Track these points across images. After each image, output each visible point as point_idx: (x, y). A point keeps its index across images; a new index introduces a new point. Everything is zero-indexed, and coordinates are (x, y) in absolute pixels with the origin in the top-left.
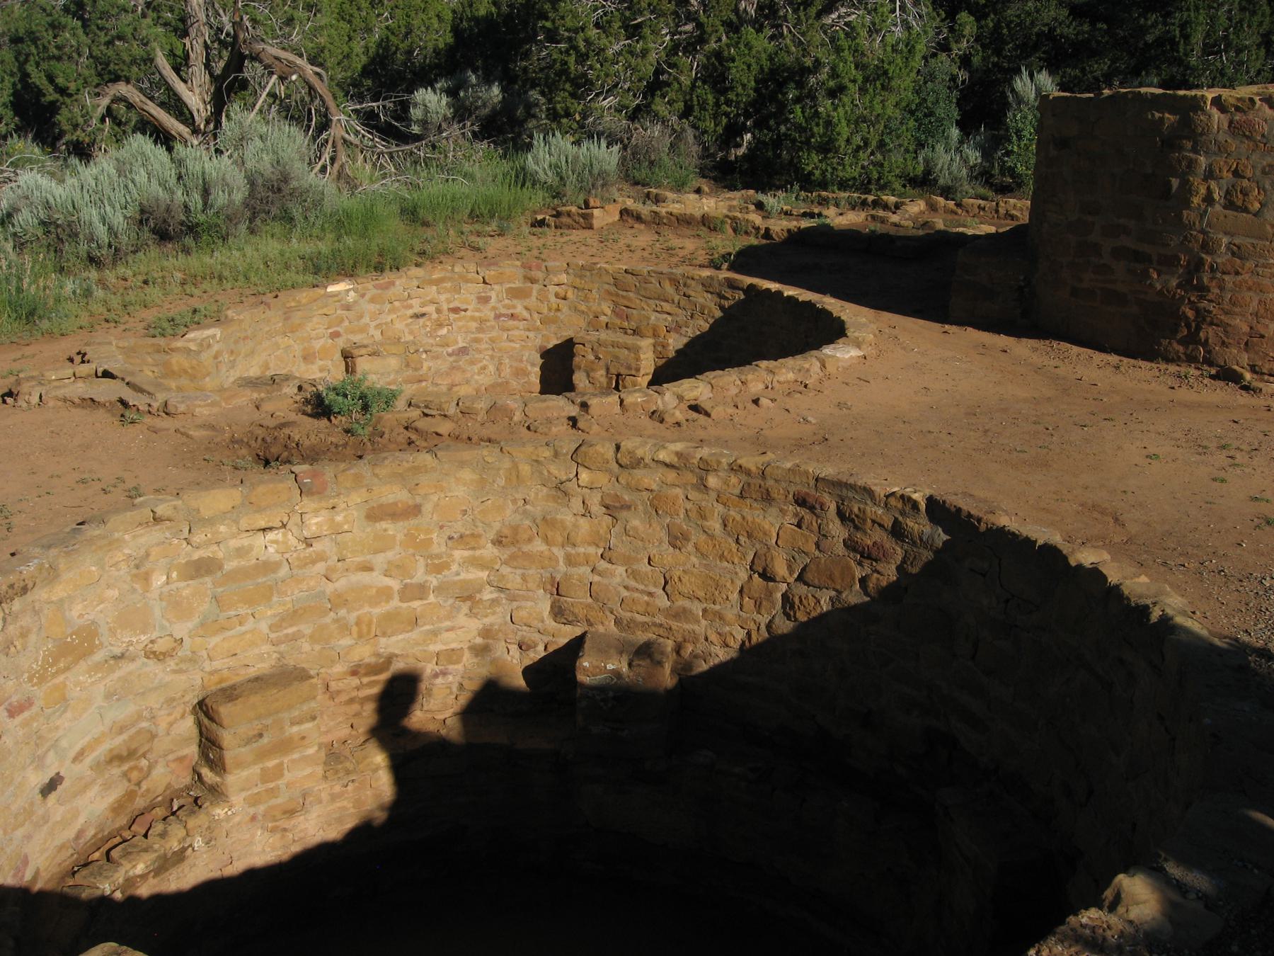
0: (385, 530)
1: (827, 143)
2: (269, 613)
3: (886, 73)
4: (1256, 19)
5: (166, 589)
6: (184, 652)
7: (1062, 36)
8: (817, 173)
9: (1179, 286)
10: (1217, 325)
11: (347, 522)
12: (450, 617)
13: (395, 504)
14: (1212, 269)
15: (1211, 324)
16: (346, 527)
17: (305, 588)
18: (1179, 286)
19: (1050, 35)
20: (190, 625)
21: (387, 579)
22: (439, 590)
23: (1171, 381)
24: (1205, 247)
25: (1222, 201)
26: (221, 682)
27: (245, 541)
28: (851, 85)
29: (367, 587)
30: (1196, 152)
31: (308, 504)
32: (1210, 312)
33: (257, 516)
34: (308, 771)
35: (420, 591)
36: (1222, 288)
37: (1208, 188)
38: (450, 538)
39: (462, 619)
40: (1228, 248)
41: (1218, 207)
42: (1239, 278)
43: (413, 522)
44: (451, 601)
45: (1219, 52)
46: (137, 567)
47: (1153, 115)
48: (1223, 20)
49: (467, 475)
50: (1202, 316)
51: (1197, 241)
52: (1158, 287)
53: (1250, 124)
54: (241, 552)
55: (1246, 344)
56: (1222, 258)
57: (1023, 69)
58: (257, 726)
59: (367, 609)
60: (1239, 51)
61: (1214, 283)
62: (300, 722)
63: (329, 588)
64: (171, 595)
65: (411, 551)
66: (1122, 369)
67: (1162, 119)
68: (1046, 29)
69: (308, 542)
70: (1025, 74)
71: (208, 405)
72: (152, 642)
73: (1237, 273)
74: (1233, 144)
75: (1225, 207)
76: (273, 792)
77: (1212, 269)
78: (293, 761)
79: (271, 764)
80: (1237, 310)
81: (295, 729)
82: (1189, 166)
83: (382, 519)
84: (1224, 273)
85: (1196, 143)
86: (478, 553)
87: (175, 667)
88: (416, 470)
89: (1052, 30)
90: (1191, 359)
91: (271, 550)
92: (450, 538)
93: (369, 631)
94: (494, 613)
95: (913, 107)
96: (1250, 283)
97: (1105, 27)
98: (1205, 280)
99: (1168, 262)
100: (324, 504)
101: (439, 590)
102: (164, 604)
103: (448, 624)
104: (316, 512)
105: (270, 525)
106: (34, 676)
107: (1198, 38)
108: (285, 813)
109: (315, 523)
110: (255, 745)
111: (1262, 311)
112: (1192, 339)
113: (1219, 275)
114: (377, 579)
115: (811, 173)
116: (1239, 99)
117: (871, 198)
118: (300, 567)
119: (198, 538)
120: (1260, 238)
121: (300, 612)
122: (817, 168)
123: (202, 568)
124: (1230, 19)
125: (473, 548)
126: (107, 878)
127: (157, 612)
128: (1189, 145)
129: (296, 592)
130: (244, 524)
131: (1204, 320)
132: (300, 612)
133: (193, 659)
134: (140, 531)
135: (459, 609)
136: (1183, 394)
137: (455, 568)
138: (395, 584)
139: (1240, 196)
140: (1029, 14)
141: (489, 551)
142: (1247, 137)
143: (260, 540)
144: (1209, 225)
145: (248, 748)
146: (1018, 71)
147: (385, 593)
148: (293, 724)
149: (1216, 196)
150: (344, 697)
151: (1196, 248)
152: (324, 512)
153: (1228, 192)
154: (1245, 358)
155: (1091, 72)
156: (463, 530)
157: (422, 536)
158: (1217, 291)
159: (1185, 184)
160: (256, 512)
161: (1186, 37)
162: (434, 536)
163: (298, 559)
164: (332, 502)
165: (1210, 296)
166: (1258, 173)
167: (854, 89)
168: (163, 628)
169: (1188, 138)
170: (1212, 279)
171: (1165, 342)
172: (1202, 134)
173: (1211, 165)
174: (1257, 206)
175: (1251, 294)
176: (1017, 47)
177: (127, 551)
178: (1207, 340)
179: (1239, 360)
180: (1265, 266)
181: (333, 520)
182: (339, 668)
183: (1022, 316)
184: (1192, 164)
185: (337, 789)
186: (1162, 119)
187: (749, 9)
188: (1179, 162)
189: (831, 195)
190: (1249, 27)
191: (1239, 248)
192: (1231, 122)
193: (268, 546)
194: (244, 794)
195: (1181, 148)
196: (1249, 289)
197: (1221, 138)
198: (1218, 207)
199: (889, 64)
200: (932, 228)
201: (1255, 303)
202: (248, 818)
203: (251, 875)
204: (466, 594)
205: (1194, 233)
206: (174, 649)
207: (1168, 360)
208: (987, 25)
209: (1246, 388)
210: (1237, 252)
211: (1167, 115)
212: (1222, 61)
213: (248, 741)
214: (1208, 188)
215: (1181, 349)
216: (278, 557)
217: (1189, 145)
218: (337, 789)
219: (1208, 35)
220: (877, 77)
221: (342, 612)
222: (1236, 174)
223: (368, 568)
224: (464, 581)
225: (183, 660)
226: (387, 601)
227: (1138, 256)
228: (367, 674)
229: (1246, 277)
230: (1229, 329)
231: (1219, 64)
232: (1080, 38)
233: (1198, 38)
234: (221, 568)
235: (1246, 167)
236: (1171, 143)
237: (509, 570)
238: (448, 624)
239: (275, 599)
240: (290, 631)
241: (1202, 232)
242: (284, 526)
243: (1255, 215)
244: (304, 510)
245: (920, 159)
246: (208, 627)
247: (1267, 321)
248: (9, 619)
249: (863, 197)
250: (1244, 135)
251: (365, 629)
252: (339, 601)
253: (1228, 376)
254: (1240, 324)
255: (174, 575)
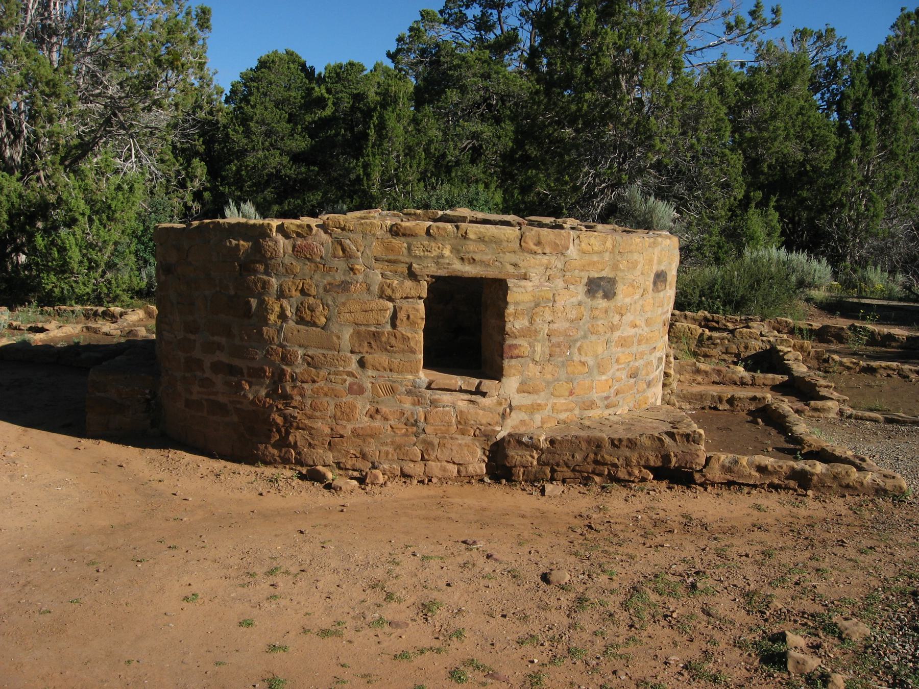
1: (63, 265)
3: (109, 207)
4: (415, 162)
7: (286, 176)
8: (57, 290)
9: (268, 395)
10: (303, 429)
14: (293, 380)
15: (298, 428)
18: (267, 395)
19: (276, 175)
23: (262, 486)
24: (284, 359)
25: (294, 317)
28: (80, 218)
30: (268, 274)
32: (295, 418)
36: (303, 396)
37: (281, 306)
40: (304, 360)
41: (291, 323)
42: (316, 385)
45: (393, 186)
47: (230, 242)
48: (393, 163)
50: (289, 421)
51: (277, 354)
52: (251, 397)
53: (309, 247)
55: (330, 444)
56: (300, 368)
57: (230, 201)
60: (406, 184)
61: (295, 391)
66: (222, 477)
67: (237, 245)
68: (274, 171)
70: (232, 205)
73: (314, 381)
74: (298, 267)
75: (297, 323)
77: (293, 380)
80: (318, 414)
82: (263, 288)
84: (303, 382)
85: (267, 266)
89: (278, 171)
90: (285, 461)
95: (140, 233)
96: (326, 389)
97: (316, 169)
98: (288, 389)
99: (256, 374)
107: (376, 175)
111: (339, 414)
112: (283, 443)
113: (299, 384)
115: (52, 291)
116: (299, 226)
117: (101, 309)
120: (330, 349)
122: (56, 287)
124: (398, 161)
128: (261, 268)
131: (291, 425)
136: (273, 501)
139: (308, 312)
140: (259, 160)
142: (309, 259)
144: (285, 339)
146: (227, 203)
149: (289, 313)
151: (277, 359)
153: (298, 309)
154: (330, 457)
155: (309, 202)
158: (298, 398)
159: (262, 303)
161: (368, 175)
165: (294, 403)
166: (321, 290)
167: (83, 221)
169: (260, 262)
170: (294, 387)
171: (262, 447)
172: (271, 258)
173: (281, 285)
174: (323, 320)
175: (328, 399)
176: (254, 185)
178: (296, 443)
179: (322, 458)
180: (336, 374)
183: (151, 431)
184: (265, 285)
186: (237, 245)
187: (15, 157)
188: (256, 284)
189: (69, 308)
190: (411, 167)
191: (313, 358)
192: (294, 247)
195: (255, 272)
196: (326, 395)
197: (287, 260)
198: (291, 323)
199: (112, 200)
200: (136, 335)
201: (332, 407)
205: (275, 347)
207: (266, 463)
208: (231, 169)
209: (329, 487)
210: (311, 362)
211: (242, 242)
212: (396, 191)
214: (281, 306)
215: (276, 452)
217: (261, 268)
219: (383, 173)
220: (102, 211)
222: (303, 292)
227: (232, 370)
229: (322, 384)
230: (313, 432)
231: (393, 194)
232: (300, 177)
233: (376, 175)
235: (310, 286)
236: (247, 267)
241: (281, 345)
243: (323, 328)
245: (144, 275)
247: (344, 423)
249: (95, 309)
250: (306, 258)
253: (314, 476)
254: (322, 427)
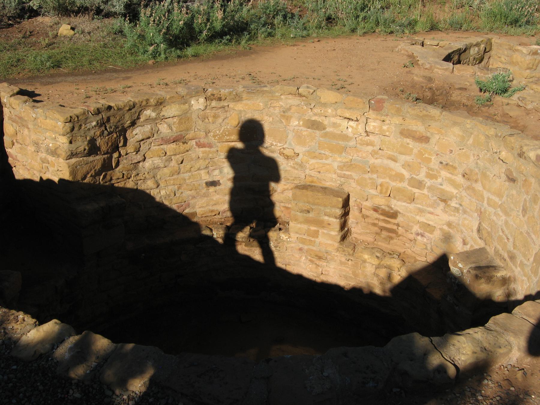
0: (408, 144)
2: (339, 160)
5: (296, 128)
6: (298, 160)
11: (388, 131)
12: (432, 206)
13: (416, 132)
16: (387, 133)
17: (360, 156)
20: (304, 149)
21: (403, 170)
22: (430, 188)
26: (312, 182)
27: (338, 121)
29: (391, 169)
31: (372, 114)
33: (346, 110)
34: (330, 242)
35: (420, 185)
38: (441, 163)
39: (439, 210)
43: (424, 145)
44: (435, 198)
46: (284, 112)
49: (456, 130)
54: (335, 125)
58: (307, 206)
59: (387, 180)
62: (329, 216)
63: (372, 161)
64: (298, 132)
65: (419, 160)
69: (367, 133)
71: (443, 69)
72: (284, 148)
76: (311, 243)
78: (323, 233)
79: (313, 228)
81: (326, 218)
83: (407, 137)
86: (454, 177)
87: (292, 165)
88: (432, 118)
91: (350, 130)
92: (441, 163)
93: (386, 192)
94: (455, 215)
100: (379, 117)
101: (430, 188)
102: (294, 134)
103: (431, 210)
104: (375, 120)
105: (351, 117)
106: (217, 135)
108: (316, 256)
109: (373, 125)
110: (305, 215)
114: (397, 167)
118: (361, 144)
119: (316, 110)
121: (354, 166)
123: (315, 125)
125: (452, 174)
126: (218, 231)
127: (290, 137)
129: (355, 155)
130: (339, 112)
132: (354, 166)
133: (301, 166)
134: (290, 96)
135: (438, 205)
137: (440, 180)
138: (406, 174)
141: (459, 179)
143: (345, 123)
145: (301, 214)
147: (400, 177)
148: (325, 215)
150: (370, 221)
152: (378, 121)
156: (448, 162)
157: (426, 156)
160: (346, 108)
162: (433, 158)
163: (361, 140)
164: (383, 118)
168: (290, 144)
177: (281, 103)
181: (382, 127)
182: (368, 204)
185: (343, 259)
193: (350, 128)
194: (298, 236)
202: (298, 248)
203: (300, 277)
204: (443, 198)
206: (293, 157)
213: (302, 211)
216: (351, 135)
218: (343, 259)
221: (375, 176)
223: (395, 160)
224: (443, 190)
225: (297, 163)
226: (400, 182)
228: (382, 214)
234: (324, 129)
237: (465, 194)
238: (431, 210)
239: (344, 154)
240: (347, 173)
242: (357, 120)
244: (368, 116)
246: (312, 154)
248: (208, 107)
251: (384, 191)
252: (373, 169)
255: (301, 123)
